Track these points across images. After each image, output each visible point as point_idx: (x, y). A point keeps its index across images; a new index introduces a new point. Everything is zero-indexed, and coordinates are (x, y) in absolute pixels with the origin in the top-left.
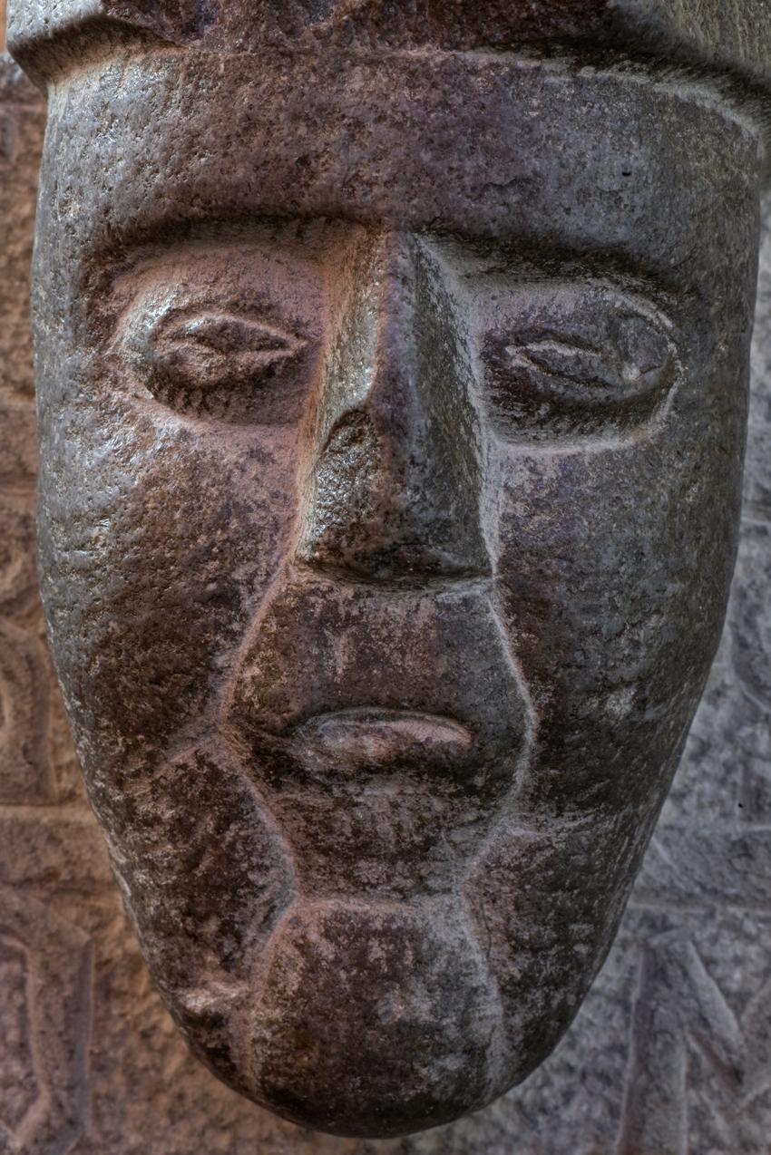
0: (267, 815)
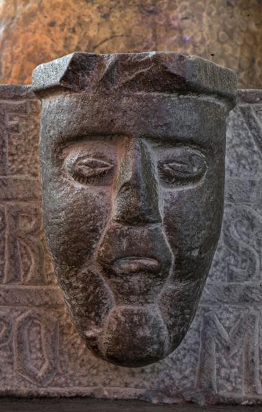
0: (107, 286)
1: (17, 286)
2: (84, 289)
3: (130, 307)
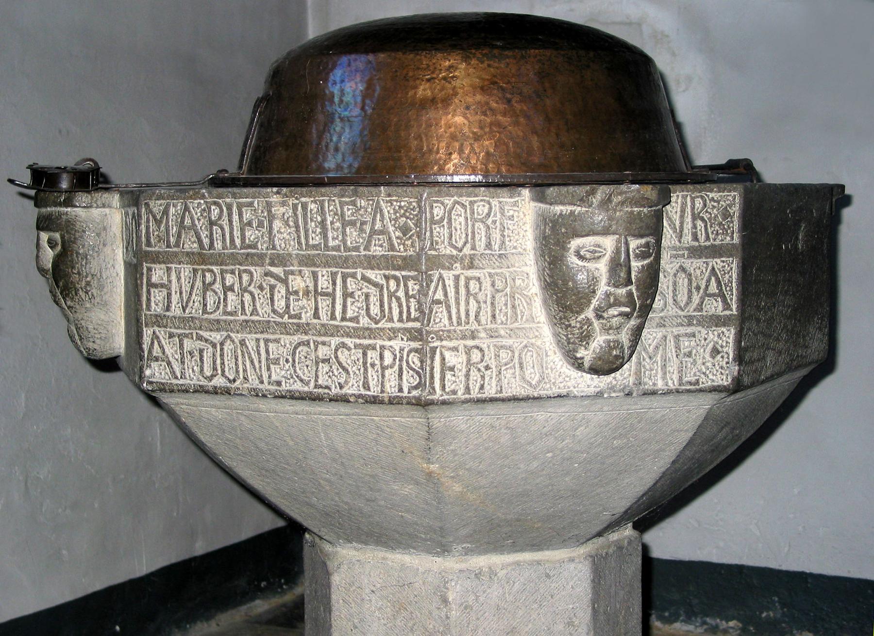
0: (596, 324)
1: (516, 325)
2: (581, 328)
3: (608, 337)
